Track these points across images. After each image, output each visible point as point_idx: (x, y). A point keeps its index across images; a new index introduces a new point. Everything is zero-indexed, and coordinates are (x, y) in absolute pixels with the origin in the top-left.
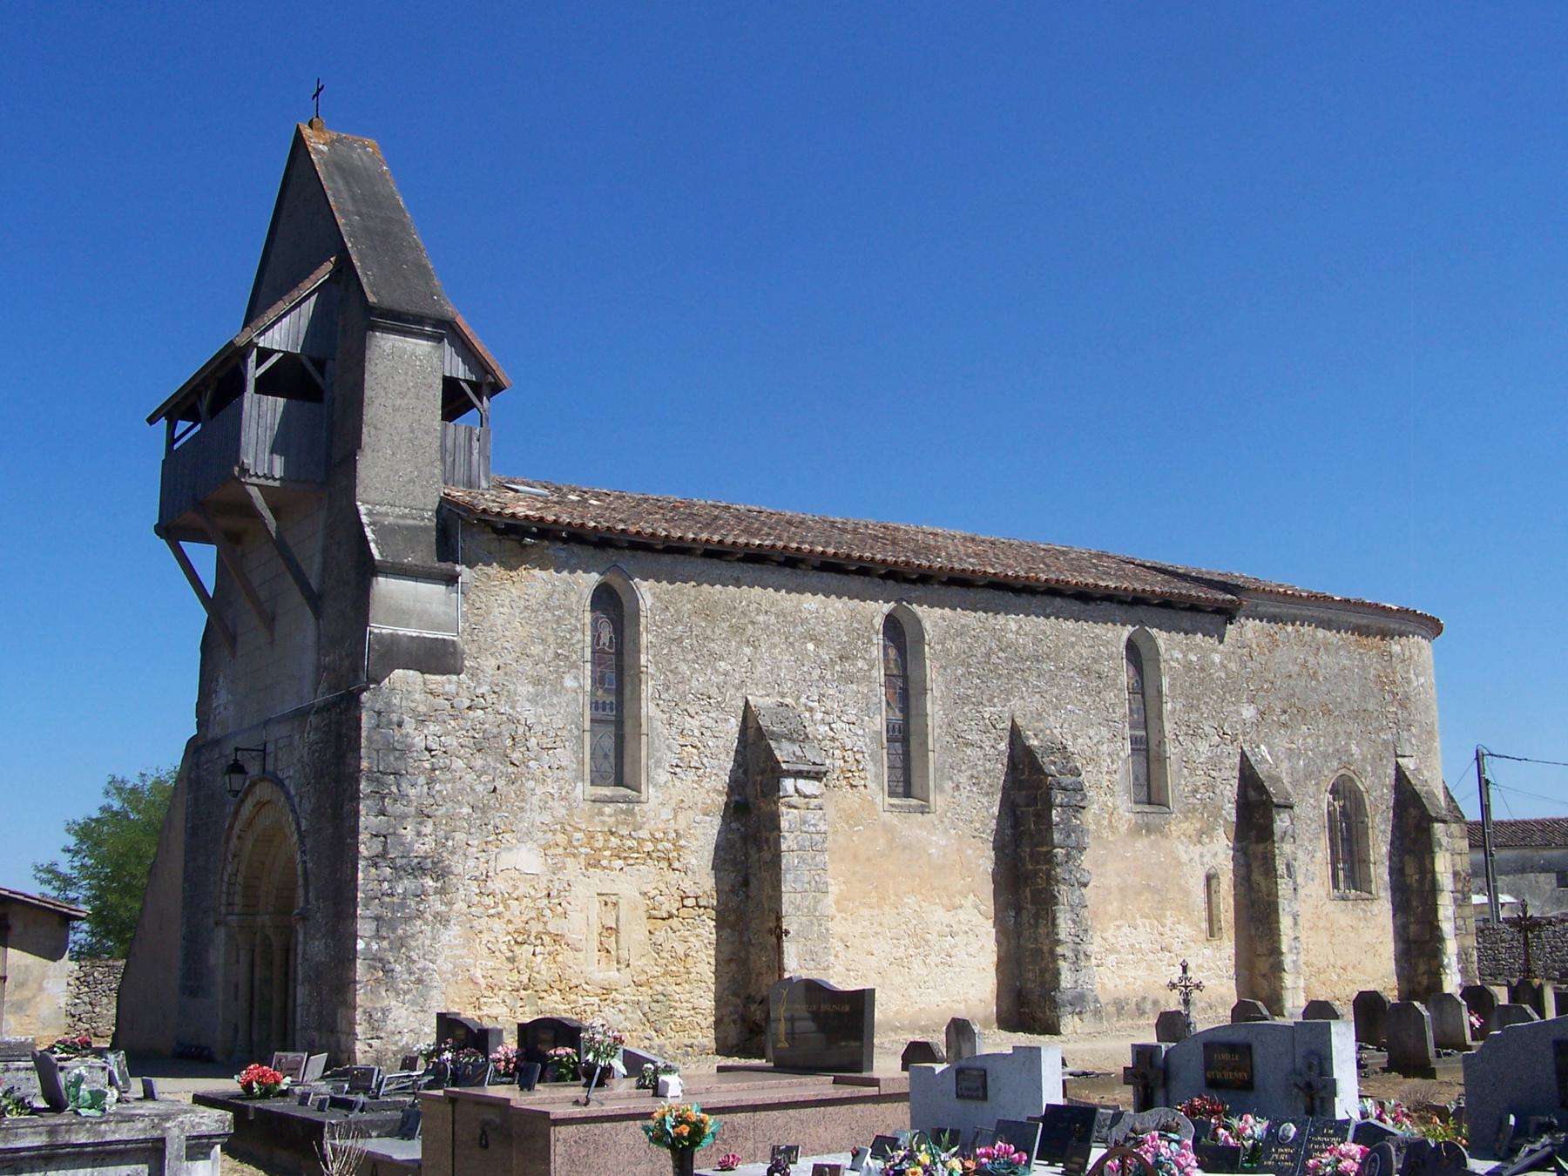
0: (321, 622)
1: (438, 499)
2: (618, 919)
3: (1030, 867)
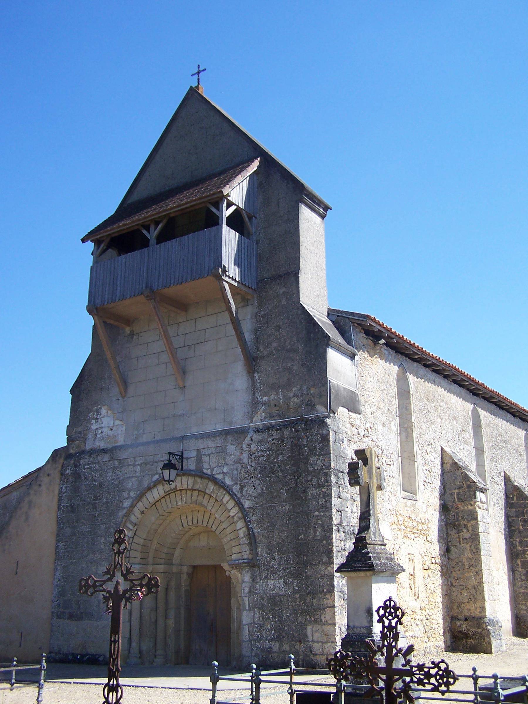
0: (256, 375)
1: (327, 310)
2: (414, 569)
3: (519, 548)
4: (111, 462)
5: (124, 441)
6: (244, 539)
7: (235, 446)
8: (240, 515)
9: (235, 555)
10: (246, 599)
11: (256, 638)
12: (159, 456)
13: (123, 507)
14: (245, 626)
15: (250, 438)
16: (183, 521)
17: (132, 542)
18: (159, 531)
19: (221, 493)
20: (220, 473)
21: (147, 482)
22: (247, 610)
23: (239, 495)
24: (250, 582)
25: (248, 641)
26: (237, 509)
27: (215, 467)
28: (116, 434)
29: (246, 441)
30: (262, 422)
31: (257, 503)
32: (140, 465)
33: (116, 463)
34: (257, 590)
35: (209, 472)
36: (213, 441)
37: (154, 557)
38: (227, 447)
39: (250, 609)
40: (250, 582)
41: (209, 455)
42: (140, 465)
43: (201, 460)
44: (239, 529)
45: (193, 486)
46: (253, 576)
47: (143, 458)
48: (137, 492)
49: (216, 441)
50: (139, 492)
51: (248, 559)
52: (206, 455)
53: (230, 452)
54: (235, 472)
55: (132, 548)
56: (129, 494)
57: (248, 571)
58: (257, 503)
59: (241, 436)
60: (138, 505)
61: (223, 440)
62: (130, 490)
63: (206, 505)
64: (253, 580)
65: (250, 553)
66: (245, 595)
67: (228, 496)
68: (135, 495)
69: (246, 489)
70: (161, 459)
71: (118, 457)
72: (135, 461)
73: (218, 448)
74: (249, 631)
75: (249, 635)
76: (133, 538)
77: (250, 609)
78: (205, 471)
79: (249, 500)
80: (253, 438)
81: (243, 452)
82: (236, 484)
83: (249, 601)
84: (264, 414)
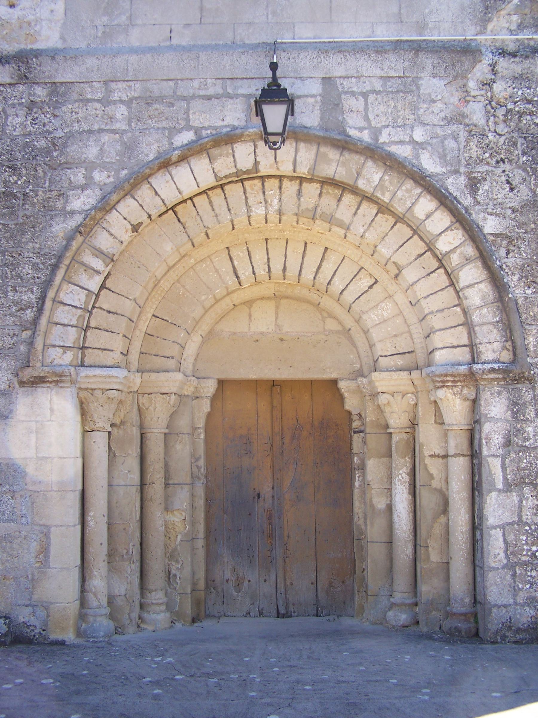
4: (21, 88)
5: (62, 38)
6: (485, 311)
7: (446, 82)
8: (470, 250)
9: (444, 351)
10: (497, 462)
11: (527, 558)
12: (196, 84)
13: (68, 209)
14: (493, 532)
15: (490, 68)
16: (236, 263)
17: (93, 307)
18: (165, 285)
19: (407, 191)
20: (402, 142)
21: (155, 147)
22: (499, 491)
23: (467, 201)
24: (507, 421)
25: (504, 567)
26: (460, 236)
27: (387, 126)
28: (31, 17)
29: (478, 75)
30: (512, 34)
31: (520, 225)
32: (128, 103)
33: (40, 92)
34: (527, 439)
35: (366, 137)
36: (376, 61)
37: (141, 353)
38: (421, 82)
39: (508, 487)
40: (507, 421)
41: (365, 95)
42: (128, 103)
43: (338, 105)
44: (468, 287)
45: (313, 169)
46: (516, 404)
47: (138, 85)
48: (117, 171)
49: (387, 63)
50: (125, 172)
51: (498, 361)
52: (353, 94)
53: (430, 95)
54: (451, 144)
55: (93, 324)
56: (89, 178)
57: (499, 393)
58: (520, 225)
59: (463, 58)
60: (121, 207)
61: (407, 64)
62: (90, 167)
63: (347, 221)
64: (515, 415)
65: (504, 348)
66: (493, 451)
67: (431, 201)
68: (112, 179)
69: (486, 187)
70: (202, 93)
71: (49, 77)
72: (109, 91)
73: (393, 81)
74: (505, 541)
75: (506, 552)
76: (98, 295)
77: (508, 487)
78: (352, 132)
79: (497, 215)
80: (498, 68)
81: (468, 98)
82: (456, 172)
83: (504, 468)
84: (515, 18)
